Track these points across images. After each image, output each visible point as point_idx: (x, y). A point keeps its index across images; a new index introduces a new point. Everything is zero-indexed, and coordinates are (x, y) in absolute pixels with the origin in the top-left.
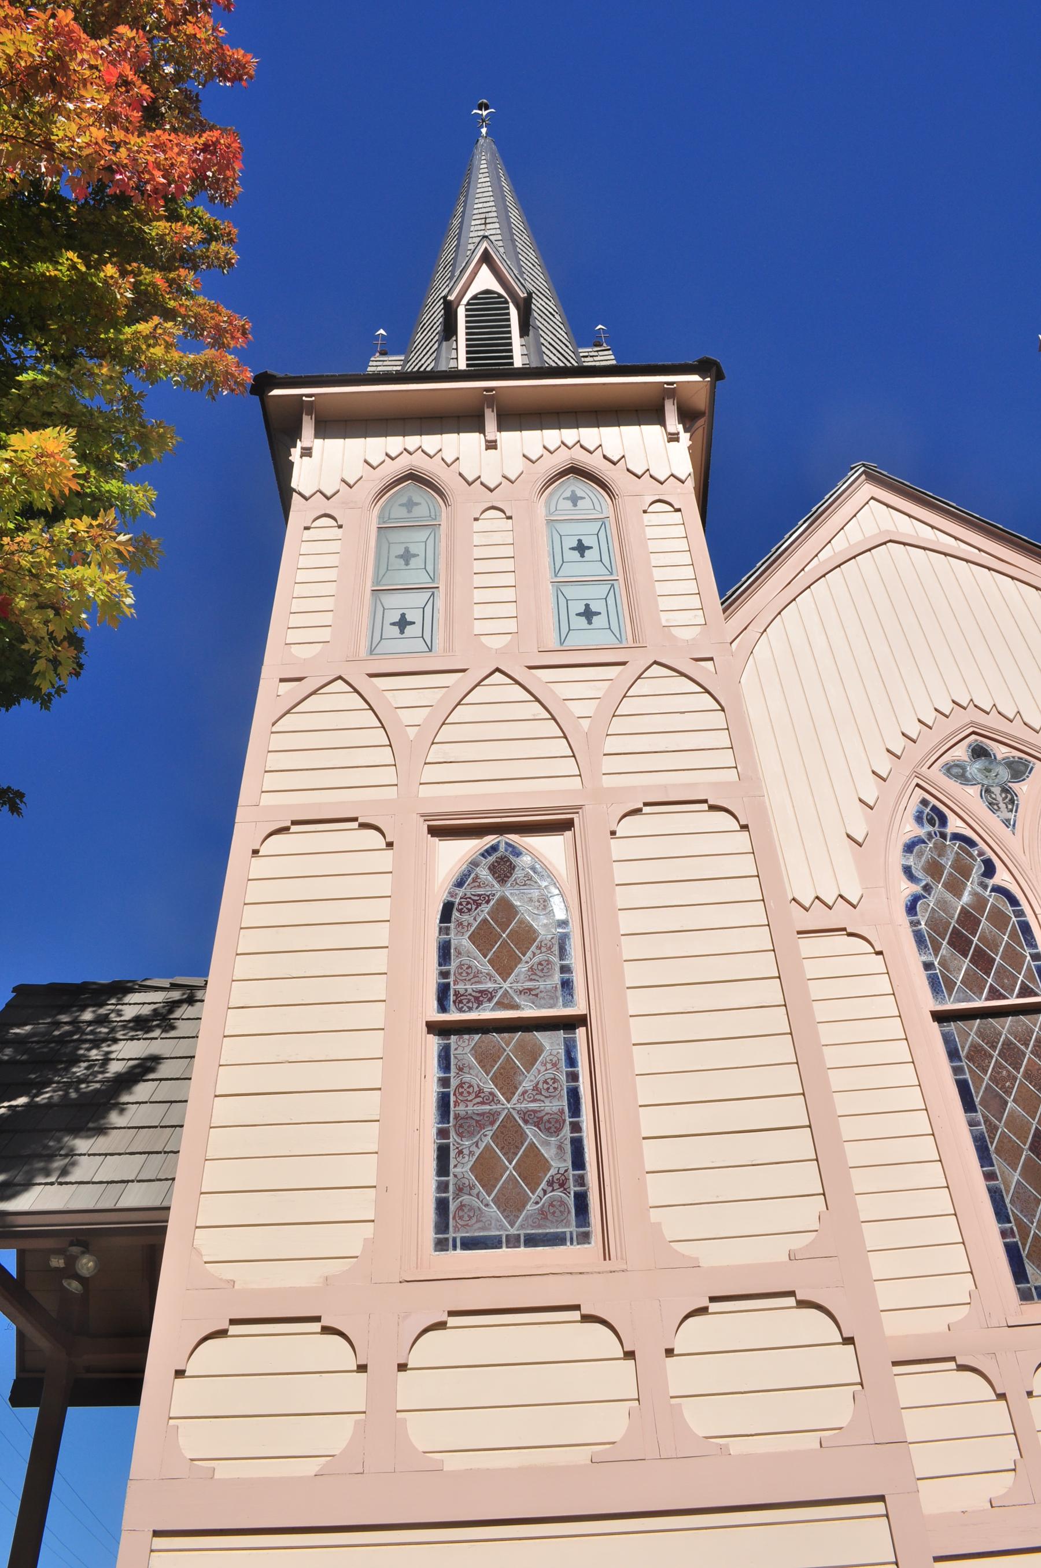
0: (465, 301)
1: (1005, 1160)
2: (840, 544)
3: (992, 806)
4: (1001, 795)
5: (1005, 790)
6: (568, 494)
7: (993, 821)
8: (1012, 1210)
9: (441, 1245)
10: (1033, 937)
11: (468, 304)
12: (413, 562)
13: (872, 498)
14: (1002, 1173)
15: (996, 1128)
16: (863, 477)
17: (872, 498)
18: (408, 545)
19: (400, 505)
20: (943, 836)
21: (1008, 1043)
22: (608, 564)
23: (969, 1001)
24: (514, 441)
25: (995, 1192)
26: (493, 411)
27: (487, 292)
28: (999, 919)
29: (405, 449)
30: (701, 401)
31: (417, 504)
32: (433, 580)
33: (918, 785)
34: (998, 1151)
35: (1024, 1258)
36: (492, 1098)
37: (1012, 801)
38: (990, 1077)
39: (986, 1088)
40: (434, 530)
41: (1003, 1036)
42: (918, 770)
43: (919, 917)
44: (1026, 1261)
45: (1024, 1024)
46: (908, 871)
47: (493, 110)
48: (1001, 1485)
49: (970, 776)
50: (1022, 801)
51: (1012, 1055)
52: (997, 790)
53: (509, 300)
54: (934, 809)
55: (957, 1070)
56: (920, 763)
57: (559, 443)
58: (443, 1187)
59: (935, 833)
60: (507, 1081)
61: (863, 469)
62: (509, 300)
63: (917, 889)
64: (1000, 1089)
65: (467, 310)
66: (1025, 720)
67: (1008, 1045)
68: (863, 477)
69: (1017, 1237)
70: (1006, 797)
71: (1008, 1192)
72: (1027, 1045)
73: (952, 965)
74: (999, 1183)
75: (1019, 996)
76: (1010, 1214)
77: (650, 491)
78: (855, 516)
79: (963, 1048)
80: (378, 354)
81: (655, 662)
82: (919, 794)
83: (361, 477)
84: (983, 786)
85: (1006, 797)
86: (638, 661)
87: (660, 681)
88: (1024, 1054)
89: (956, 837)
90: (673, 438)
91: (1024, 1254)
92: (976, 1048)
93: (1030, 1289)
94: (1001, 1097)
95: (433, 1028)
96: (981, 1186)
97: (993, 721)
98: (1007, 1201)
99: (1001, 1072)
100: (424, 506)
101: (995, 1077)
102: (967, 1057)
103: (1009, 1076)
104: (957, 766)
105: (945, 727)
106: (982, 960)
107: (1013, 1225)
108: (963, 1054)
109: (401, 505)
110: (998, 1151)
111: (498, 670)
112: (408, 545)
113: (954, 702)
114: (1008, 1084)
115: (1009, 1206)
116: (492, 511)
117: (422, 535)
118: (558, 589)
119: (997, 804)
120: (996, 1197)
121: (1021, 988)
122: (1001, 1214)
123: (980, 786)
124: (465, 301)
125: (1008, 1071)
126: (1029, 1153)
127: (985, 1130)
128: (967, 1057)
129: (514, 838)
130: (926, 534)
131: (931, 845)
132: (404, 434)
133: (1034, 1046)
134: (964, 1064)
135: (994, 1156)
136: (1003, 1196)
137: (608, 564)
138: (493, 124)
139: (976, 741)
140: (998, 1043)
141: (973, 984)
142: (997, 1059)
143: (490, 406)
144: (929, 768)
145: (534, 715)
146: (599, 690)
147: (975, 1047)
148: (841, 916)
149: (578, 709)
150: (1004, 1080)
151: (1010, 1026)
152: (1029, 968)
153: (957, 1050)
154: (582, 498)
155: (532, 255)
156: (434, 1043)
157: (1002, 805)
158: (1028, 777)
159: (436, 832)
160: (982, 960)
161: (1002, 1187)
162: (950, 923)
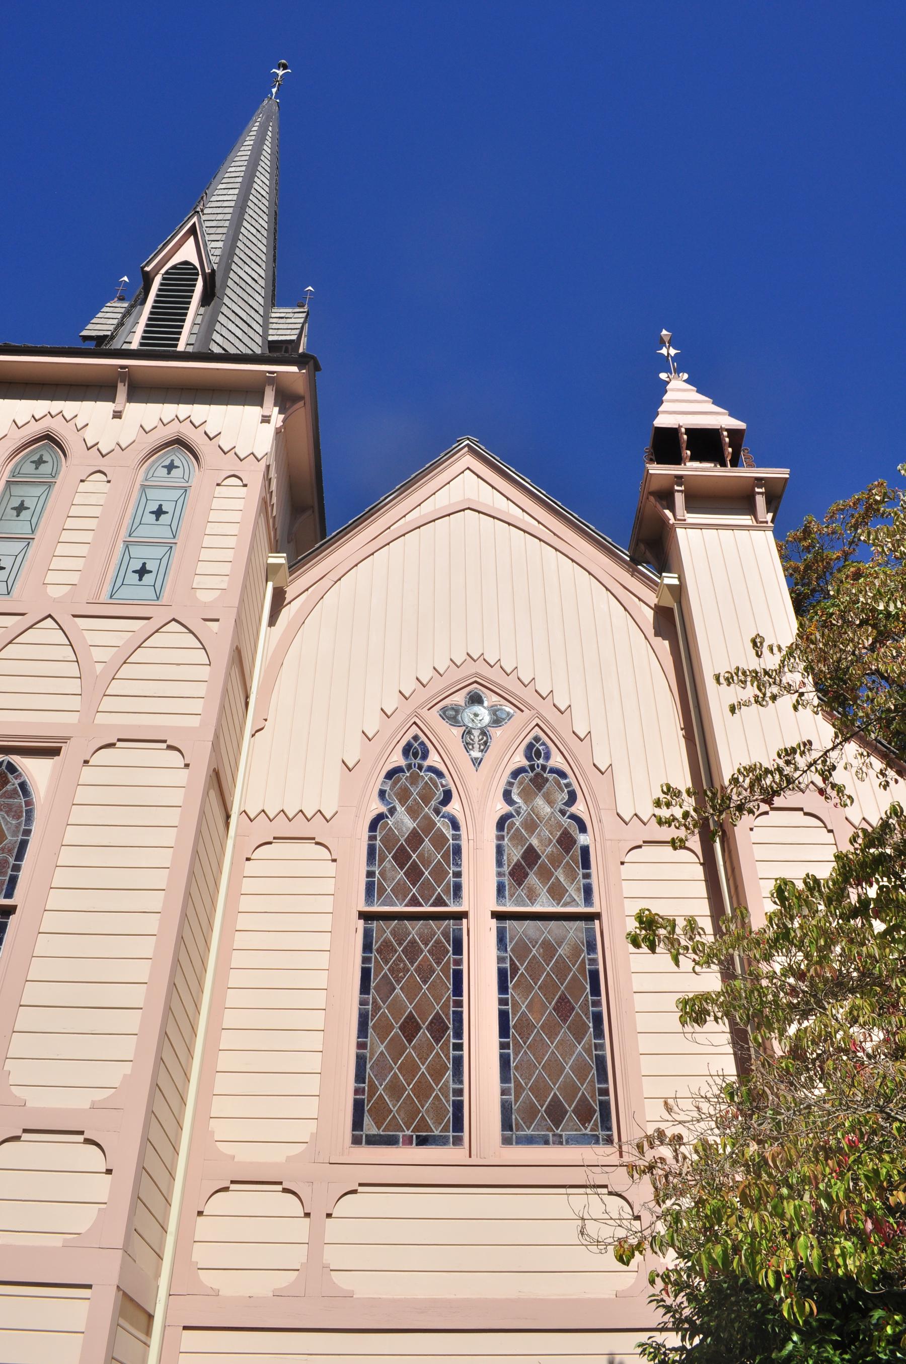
0: (163, 271)
1: (378, 1034)
2: (428, 509)
3: (468, 746)
4: (478, 737)
5: (483, 733)
6: (167, 463)
8: (369, 1074)
10: (460, 858)
11: (167, 273)
13: (468, 468)
14: (372, 1044)
15: (380, 1008)
16: (466, 449)
17: (468, 468)
18: (24, 498)
19: (31, 462)
20: (420, 767)
21: (413, 942)
22: (174, 530)
23: (392, 905)
25: (361, 1058)
26: (124, 385)
27: (186, 263)
29: (49, 413)
30: (300, 387)
31: (45, 462)
32: (33, 532)
33: (415, 723)
34: (374, 1027)
35: (366, 1112)
37: (486, 743)
38: (389, 968)
39: (383, 976)
40: (50, 486)
41: (411, 936)
42: (419, 711)
43: (378, 833)
44: (366, 1114)
45: (431, 927)
46: (382, 794)
47: (289, 71)
49: (460, 719)
50: (492, 745)
51: (412, 951)
52: (476, 733)
53: (200, 273)
54: (422, 743)
55: (365, 960)
56: (421, 706)
57: (174, 416)
59: (415, 765)
61: (468, 442)
62: (200, 273)
63: (383, 809)
64: (394, 978)
65: (164, 279)
66: (177, 753)
67: (412, 943)
68: (466, 449)
69: (366, 1095)
70: (482, 739)
71: (371, 1059)
72: (426, 945)
73: (389, 874)
74: (367, 1052)
75: (432, 905)
76: (367, 1077)
77: (229, 464)
78: (449, 483)
79: (377, 942)
80: (116, 299)
81: (174, 620)
82: (414, 730)
83: (6, 435)
84: (467, 728)
85: (482, 739)
86: (160, 615)
87: (174, 636)
88: (422, 951)
89: (431, 769)
90: (266, 419)
91: (366, 1109)
92: (386, 943)
93: (362, 1136)
94: (392, 984)
96: (353, 1051)
97: (495, 675)
98: (368, 1066)
99: (399, 965)
100: (50, 464)
101: (393, 968)
102: (377, 951)
103: (404, 968)
104: (453, 709)
105: (456, 675)
106: (414, 874)
107: (366, 1086)
108: (375, 947)
109: (32, 462)
110: (374, 1027)
111: (50, 616)
112: (24, 498)
113: (468, 654)
114: (401, 974)
115: (368, 1070)
116: (98, 474)
117: (38, 491)
118: (127, 546)
119: (473, 745)
120: (361, 1062)
121: (436, 899)
122: (360, 1076)
123: (464, 728)
124: (163, 271)
125: (405, 965)
126: (398, 1030)
127: (370, 1009)
128: (377, 951)
129: (16, 759)
130: (501, 504)
131: (408, 775)
132: (52, 399)
133: (432, 946)
134: (373, 955)
135: (370, 1030)
136: (366, 1062)
137: (174, 530)
138: (285, 86)
139: (477, 688)
140: (404, 941)
141: (400, 891)
142: (399, 954)
143: (123, 381)
144: (429, 710)
145: (64, 657)
146: (118, 640)
148: (316, 828)
149: (97, 654)
150: (399, 971)
151: (419, 928)
152: (448, 884)
153: (372, 943)
154: (177, 467)
155: (263, 222)
157: (477, 746)
158: (506, 723)
160: (414, 874)
161: (368, 1055)
162: (400, 840)
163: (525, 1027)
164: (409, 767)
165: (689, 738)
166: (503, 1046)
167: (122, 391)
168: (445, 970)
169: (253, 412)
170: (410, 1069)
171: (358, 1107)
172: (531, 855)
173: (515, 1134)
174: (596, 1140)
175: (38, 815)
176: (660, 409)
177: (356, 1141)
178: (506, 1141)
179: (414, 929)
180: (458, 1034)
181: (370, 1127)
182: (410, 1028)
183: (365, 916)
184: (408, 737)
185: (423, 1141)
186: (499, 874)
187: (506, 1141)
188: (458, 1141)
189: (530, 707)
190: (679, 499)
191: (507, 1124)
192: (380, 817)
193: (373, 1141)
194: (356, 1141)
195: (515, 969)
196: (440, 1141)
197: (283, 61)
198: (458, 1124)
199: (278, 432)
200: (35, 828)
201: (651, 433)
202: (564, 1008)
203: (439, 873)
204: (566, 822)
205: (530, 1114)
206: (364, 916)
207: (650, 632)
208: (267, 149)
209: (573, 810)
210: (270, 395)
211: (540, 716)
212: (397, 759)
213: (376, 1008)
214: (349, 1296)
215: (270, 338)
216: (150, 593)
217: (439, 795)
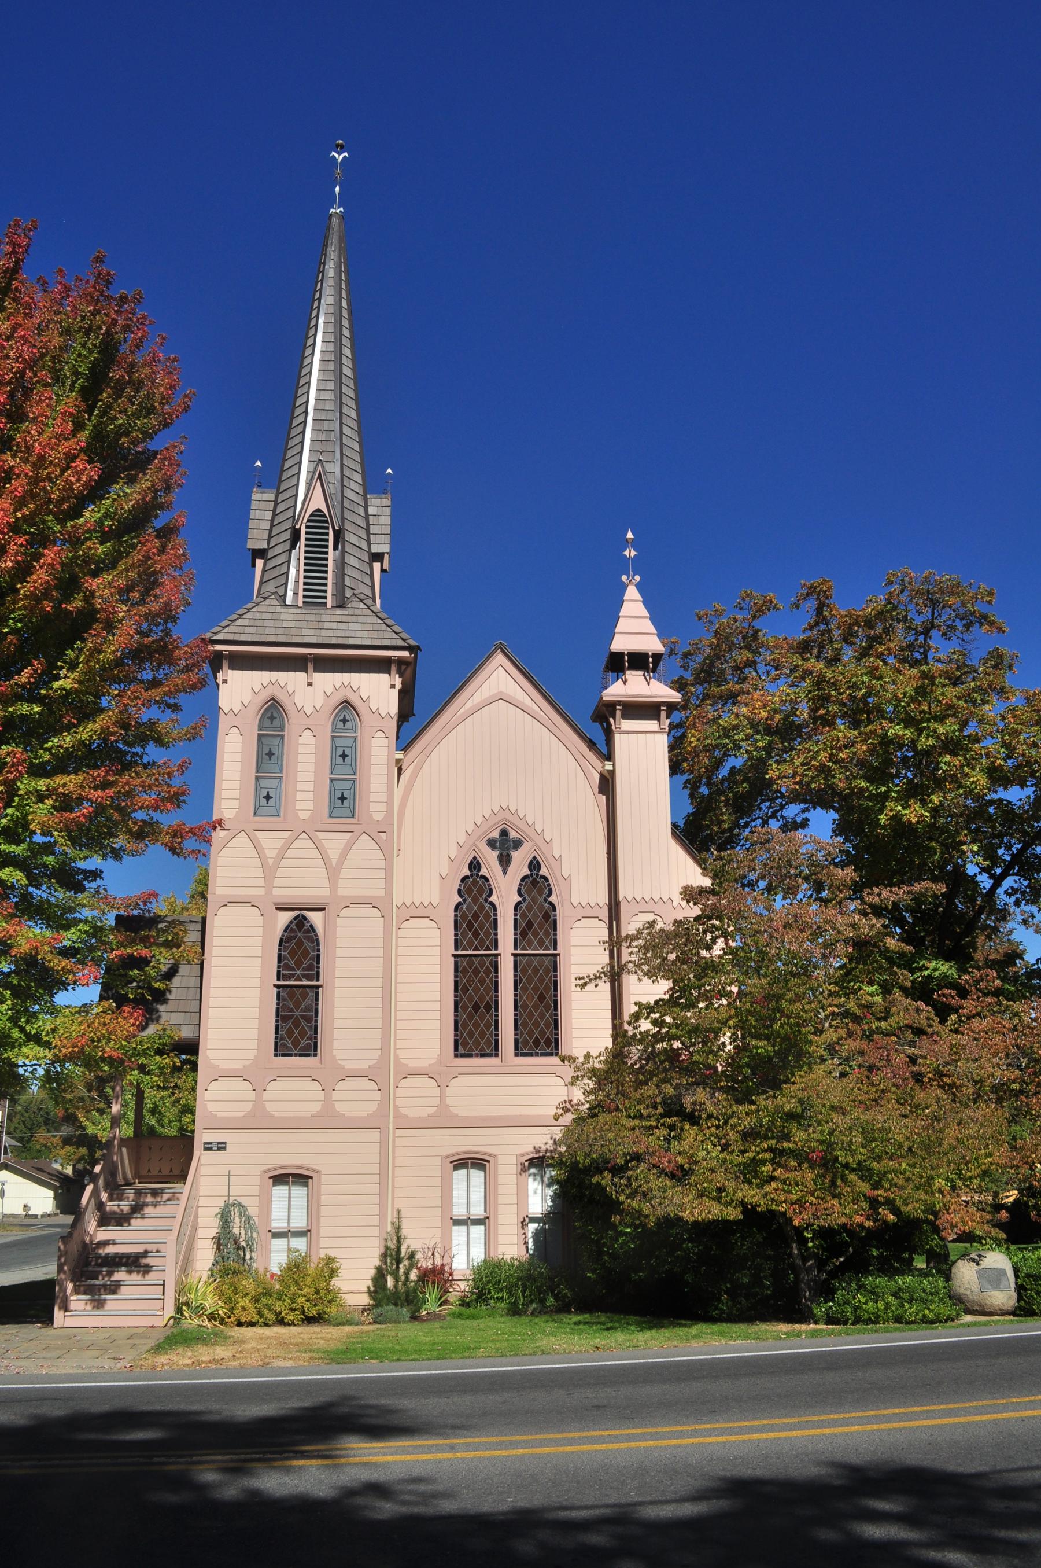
7: (497, 868)
9: (276, 1055)
12: (273, 757)
24: (319, 678)
28: (487, 916)
36: (292, 1010)
48: (432, 1110)
55: (456, 977)
58: (276, 1038)
60: (297, 1005)
63: (460, 900)
82: (474, 854)
95: (275, 986)
97: (514, 819)
106: (476, 934)
117: (276, 741)
129: (305, 913)
141: (470, 945)
147: (464, 968)
156: (275, 989)
159: (278, 909)
160: (476, 934)
163: (525, 1006)
164: (472, 875)
165: (609, 858)
166: (516, 1015)
167: (310, 667)
168: (491, 980)
169: (384, 677)
170: (476, 1025)
171: (456, 1042)
172: (530, 924)
173: (520, 1052)
174: (551, 1054)
175: (321, 941)
176: (621, 614)
177: (456, 1056)
178: (516, 1055)
179: (476, 961)
180: (497, 1010)
181: (461, 1051)
182: (476, 1007)
183: (454, 956)
184: (471, 858)
185: (483, 1056)
186: (515, 934)
187: (516, 1055)
188: (497, 1055)
189: (532, 840)
190: (618, 713)
191: (516, 1048)
192: (459, 904)
193: (463, 1056)
194: (456, 1056)
195: (521, 980)
196: (490, 1055)
197: (341, 142)
198: (497, 1049)
199: (400, 692)
200: (321, 948)
201: (607, 655)
202: (542, 998)
203: (487, 934)
204: (546, 905)
205: (526, 1043)
206: (453, 955)
207: (597, 790)
208: (597, 1512)
209: (550, 899)
210: (394, 669)
211: (536, 845)
212: (466, 872)
213: (462, 999)
214: (457, 1115)
215: (373, 550)
216: (348, 813)
217: (487, 891)
